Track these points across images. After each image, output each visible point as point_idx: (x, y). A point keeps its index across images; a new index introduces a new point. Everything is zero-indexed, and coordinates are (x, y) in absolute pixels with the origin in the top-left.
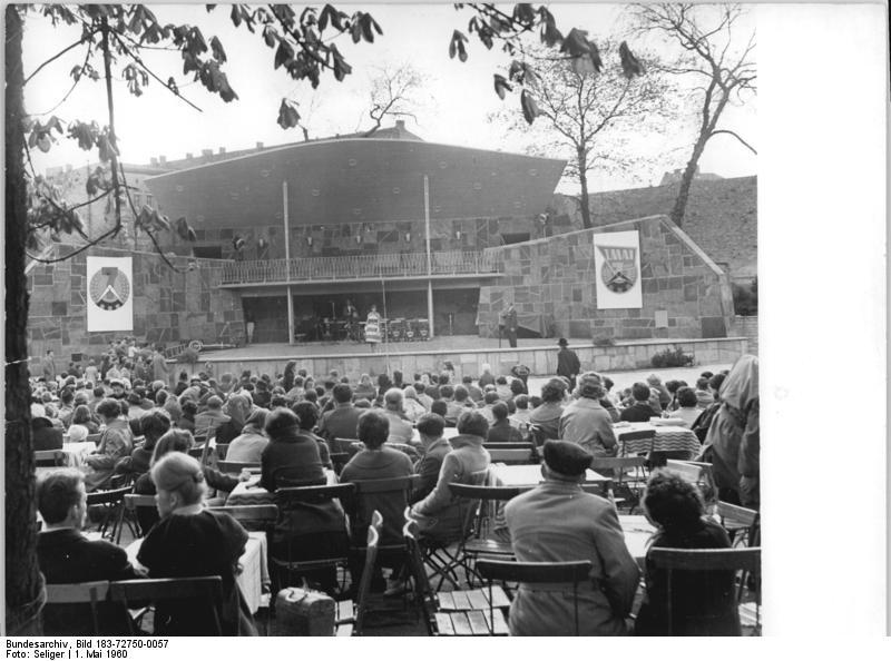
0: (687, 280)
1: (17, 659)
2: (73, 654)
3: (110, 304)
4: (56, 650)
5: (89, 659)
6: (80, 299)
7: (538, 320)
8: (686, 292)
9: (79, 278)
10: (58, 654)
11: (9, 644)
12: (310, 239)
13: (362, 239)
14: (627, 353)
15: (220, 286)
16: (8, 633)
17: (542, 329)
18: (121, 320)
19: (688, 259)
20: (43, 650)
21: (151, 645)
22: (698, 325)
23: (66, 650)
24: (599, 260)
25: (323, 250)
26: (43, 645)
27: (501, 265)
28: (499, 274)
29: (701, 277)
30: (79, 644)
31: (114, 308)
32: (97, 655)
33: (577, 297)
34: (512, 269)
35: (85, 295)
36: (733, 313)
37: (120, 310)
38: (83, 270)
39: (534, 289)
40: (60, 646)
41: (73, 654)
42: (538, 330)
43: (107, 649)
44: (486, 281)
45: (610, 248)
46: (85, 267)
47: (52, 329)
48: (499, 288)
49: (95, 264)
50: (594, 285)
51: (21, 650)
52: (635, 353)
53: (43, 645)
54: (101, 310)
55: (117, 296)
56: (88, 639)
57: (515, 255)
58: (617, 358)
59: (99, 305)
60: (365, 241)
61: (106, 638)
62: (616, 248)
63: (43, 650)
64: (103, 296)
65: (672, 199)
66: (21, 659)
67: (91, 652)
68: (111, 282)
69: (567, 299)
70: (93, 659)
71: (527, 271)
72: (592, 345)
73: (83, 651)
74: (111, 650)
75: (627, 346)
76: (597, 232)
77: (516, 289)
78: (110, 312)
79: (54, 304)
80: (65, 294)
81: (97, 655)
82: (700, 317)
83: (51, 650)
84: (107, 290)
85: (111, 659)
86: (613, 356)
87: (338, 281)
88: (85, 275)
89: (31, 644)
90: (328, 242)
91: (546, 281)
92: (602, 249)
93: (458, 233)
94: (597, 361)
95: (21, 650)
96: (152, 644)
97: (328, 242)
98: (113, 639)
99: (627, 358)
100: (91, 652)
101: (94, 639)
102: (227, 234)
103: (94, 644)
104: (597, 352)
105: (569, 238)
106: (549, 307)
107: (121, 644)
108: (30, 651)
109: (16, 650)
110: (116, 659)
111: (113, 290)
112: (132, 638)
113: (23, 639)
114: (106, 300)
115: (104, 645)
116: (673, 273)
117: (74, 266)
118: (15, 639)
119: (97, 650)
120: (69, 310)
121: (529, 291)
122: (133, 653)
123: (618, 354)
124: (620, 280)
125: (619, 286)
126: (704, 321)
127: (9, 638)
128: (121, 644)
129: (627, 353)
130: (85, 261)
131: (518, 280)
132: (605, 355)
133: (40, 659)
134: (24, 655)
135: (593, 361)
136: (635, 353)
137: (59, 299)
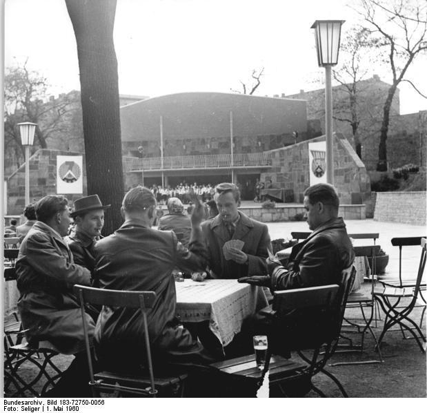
0: (346, 170)
1: (10, 412)
2: (45, 409)
3: (70, 180)
4: (34, 406)
5: (55, 412)
6: (53, 177)
7: (281, 193)
8: (346, 177)
9: (53, 167)
10: (36, 409)
11: (5, 402)
12: (184, 147)
13: (211, 147)
14: (283, 212)
15: (131, 171)
16: (5, 396)
17: (282, 198)
18: (77, 188)
19: (346, 158)
20: (27, 406)
21: (94, 403)
22: (349, 197)
23: (41, 406)
24: (311, 158)
25: (192, 152)
26: (27, 403)
27: (271, 161)
28: (269, 166)
29: (352, 169)
30: (49, 403)
31: (72, 182)
32: (60, 409)
33: (303, 180)
34: (276, 163)
35: (56, 175)
36: (370, 189)
37: (75, 183)
38: (55, 163)
39: (286, 174)
40: (37, 403)
41: (45, 409)
42: (280, 198)
43: (66, 405)
44: (264, 170)
45: (315, 152)
46: (56, 161)
47: (38, 192)
48: (270, 174)
49: (61, 160)
50: (309, 173)
51: (13, 406)
52: (288, 212)
53: (27, 403)
54: (65, 183)
55: (74, 176)
56: (54, 399)
57: (277, 155)
58: (276, 215)
59: (64, 180)
60: (213, 147)
61: (66, 399)
62: (318, 152)
63: (27, 406)
64: (65, 176)
65: (181, 141)
66: (13, 412)
67: (56, 407)
68: (70, 168)
69: (299, 181)
70: (58, 412)
71: (282, 165)
72: (261, 207)
73: (51, 407)
74: (68, 406)
75: (283, 208)
76: (311, 142)
77: (278, 175)
78: (70, 184)
79: (39, 180)
80: (45, 175)
81: (60, 409)
82: (351, 193)
83: (32, 406)
84: (68, 173)
85: (69, 412)
86: (274, 213)
87: (221, 168)
88: (56, 165)
89: (19, 403)
90: (193, 148)
91: (291, 170)
92: (312, 152)
93: (260, 143)
94: (264, 215)
95: (13, 406)
96: (94, 402)
97: (193, 148)
98: (70, 399)
99: (283, 214)
100: (56, 407)
101: (58, 400)
102: (145, 143)
103: (59, 403)
104: (263, 211)
105: (300, 145)
106: (292, 184)
107: (75, 402)
108: (19, 407)
109: (10, 406)
110: (72, 411)
111: (72, 173)
112: (82, 399)
113: (14, 399)
114: (67, 178)
115: (64, 403)
116: (341, 166)
117: (50, 161)
118: (9, 400)
119: (60, 406)
120: (47, 182)
121: (283, 176)
122: (82, 408)
123: (278, 212)
124: (319, 170)
125: (319, 174)
126: (353, 195)
127: (5, 399)
128: (75, 402)
129: (283, 212)
130: (56, 158)
131: (279, 169)
132: (269, 213)
133: (25, 412)
134: (15, 409)
135: (261, 216)
136: (288, 212)
137: (41, 177)
